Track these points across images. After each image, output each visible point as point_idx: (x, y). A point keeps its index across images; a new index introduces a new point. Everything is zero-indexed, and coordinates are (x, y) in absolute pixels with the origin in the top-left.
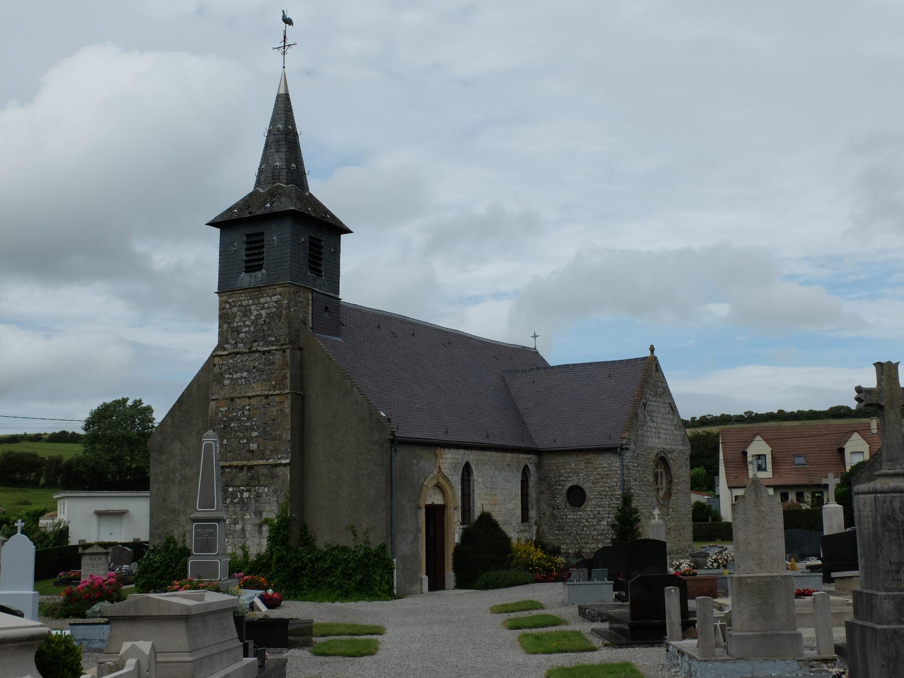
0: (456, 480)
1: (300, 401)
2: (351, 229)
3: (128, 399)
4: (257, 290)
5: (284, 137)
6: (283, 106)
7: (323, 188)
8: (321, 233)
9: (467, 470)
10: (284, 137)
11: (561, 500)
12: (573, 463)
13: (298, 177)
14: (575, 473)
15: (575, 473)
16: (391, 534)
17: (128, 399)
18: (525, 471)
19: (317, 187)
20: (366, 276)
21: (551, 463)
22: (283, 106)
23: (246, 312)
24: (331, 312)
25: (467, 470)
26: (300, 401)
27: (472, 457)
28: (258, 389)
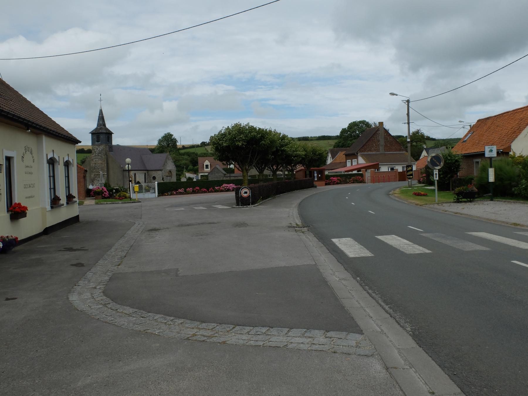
0: (133, 176)
1: (107, 164)
2: (79, 138)
3: (80, 142)
4: (99, 145)
5: (101, 118)
6: (101, 112)
7: (109, 125)
8: (109, 134)
9: (135, 174)
10: (101, 118)
11: (152, 178)
12: (153, 172)
13: (104, 125)
14: (154, 174)
15: (154, 174)
16: (124, 185)
17: (80, 142)
18: (145, 174)
19: (108, 126)
20: (116, 141)
21: (150, 172)
22: (101, 112)
23: (97, 149)
24: (111, 148)
25: (135, 174)
26: (107, 164)
27: (136, 172)
28: (100, 162)
